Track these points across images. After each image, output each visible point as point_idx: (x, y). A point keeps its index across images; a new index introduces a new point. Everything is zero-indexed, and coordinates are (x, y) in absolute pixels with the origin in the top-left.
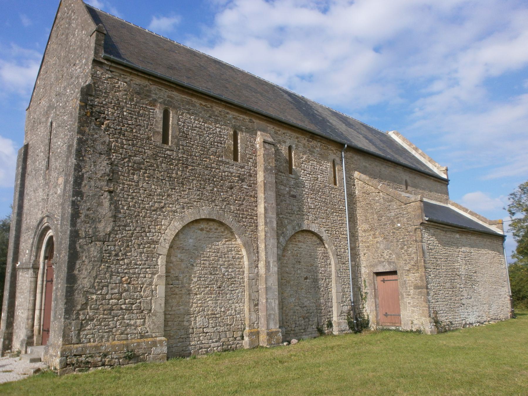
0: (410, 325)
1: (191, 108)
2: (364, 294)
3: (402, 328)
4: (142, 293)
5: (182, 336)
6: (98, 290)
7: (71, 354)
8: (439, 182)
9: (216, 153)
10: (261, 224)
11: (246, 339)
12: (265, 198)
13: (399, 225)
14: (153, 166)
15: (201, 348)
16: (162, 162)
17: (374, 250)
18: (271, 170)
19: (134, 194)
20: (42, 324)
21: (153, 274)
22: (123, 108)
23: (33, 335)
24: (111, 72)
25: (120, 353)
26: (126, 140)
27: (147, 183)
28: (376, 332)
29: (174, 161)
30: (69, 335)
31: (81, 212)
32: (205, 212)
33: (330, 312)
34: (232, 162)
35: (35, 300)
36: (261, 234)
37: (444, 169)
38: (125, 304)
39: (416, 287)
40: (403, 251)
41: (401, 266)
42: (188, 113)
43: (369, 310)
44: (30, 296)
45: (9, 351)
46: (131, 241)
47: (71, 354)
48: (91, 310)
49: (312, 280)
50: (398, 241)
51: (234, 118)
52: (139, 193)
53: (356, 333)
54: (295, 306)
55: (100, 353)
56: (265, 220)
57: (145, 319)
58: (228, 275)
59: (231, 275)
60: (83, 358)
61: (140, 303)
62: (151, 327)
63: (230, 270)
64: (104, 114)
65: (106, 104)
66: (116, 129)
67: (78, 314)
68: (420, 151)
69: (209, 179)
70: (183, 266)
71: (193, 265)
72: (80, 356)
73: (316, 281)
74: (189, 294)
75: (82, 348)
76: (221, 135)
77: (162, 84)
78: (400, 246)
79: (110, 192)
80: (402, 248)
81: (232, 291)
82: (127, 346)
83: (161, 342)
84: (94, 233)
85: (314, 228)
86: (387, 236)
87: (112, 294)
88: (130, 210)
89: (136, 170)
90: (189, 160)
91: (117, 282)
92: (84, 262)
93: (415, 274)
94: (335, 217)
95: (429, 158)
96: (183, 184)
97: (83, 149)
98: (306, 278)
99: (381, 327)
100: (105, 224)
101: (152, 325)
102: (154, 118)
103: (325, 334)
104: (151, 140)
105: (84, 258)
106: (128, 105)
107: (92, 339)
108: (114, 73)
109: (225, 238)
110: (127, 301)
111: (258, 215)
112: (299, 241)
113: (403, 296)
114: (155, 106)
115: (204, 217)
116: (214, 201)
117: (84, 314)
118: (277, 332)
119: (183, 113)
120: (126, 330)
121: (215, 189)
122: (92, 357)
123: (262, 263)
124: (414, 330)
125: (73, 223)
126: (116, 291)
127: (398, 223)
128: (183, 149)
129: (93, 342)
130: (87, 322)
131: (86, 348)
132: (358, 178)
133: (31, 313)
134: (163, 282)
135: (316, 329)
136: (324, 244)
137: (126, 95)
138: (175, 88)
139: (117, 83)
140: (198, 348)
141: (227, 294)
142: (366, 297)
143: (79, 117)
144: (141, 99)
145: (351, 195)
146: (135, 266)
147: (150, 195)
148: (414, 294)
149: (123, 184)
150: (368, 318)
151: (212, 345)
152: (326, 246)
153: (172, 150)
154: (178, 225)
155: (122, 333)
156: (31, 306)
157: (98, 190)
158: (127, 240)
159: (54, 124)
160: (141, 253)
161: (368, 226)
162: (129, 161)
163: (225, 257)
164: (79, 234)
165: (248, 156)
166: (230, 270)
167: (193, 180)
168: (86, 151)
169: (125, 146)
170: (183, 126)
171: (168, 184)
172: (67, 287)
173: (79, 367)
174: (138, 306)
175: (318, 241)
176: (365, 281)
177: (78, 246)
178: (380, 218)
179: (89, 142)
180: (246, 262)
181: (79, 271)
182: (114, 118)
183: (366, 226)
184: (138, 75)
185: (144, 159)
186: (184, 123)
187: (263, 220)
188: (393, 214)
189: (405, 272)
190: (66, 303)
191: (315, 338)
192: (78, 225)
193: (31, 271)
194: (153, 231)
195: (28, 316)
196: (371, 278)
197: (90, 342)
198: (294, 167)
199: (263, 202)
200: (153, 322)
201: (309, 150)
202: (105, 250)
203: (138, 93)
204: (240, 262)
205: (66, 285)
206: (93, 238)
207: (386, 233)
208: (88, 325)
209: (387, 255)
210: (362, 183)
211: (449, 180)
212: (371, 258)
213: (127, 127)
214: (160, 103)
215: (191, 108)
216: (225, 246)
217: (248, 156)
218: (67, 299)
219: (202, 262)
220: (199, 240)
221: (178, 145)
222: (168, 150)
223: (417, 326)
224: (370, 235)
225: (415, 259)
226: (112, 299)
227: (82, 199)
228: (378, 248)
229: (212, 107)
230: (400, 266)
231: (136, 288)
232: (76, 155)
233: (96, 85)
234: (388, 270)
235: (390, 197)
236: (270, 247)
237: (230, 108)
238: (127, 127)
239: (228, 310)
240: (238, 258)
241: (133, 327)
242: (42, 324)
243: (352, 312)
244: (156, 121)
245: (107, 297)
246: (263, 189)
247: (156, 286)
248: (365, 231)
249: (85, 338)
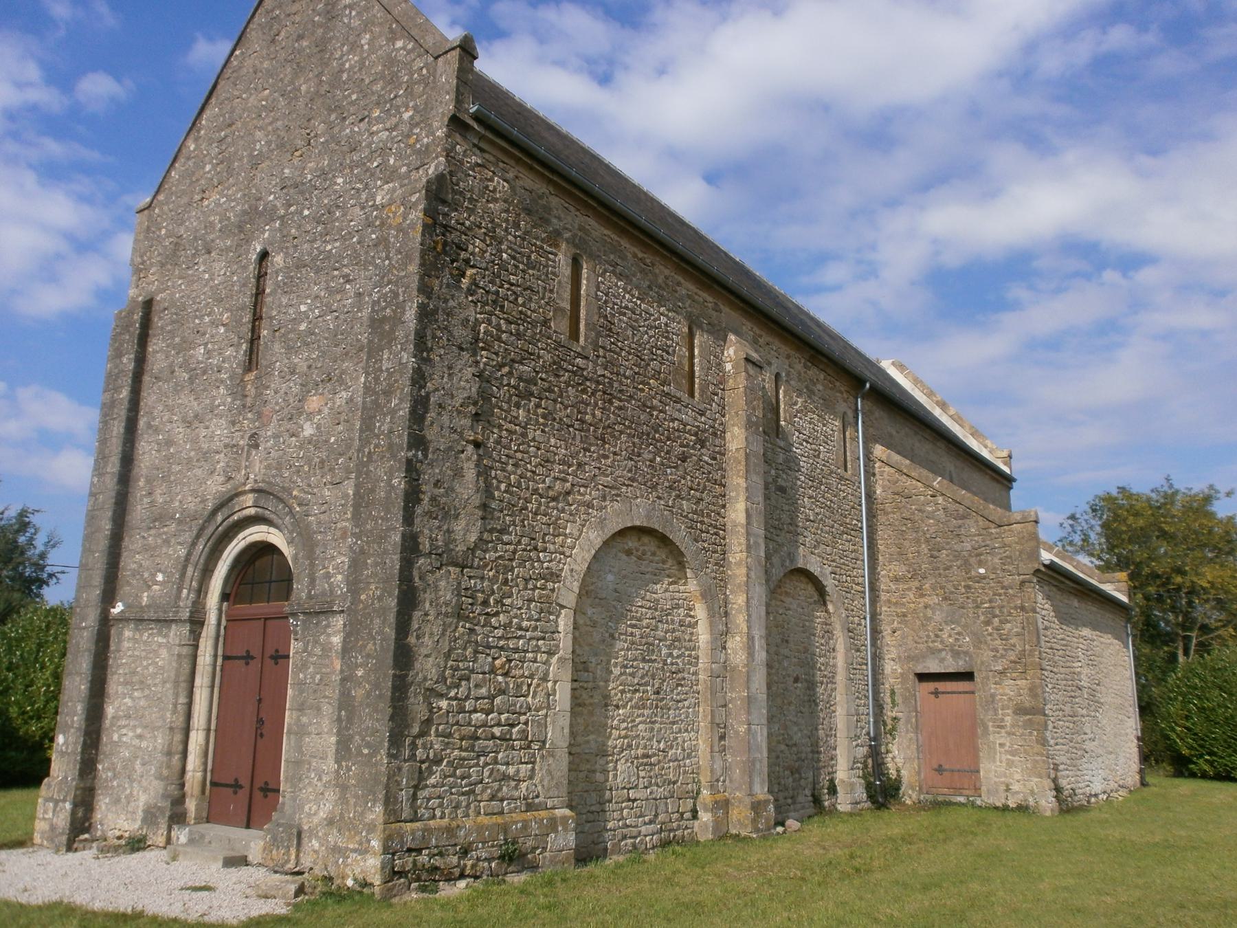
0: (1003, 795)
1: (619, 261)
2: (889, 722)
3: (986, 799)
4: (529, 699)
5: (593, 808)
6: (449, 688)
7: (402, 847)
8: (998, 481)
9: (659, 373)
10: (736, 548)
11: (705, 817)
12: (747, 489)
13: (982, 571)
14: (553, 391)
15: (624, 837)
16: (568, 384)
17: (918, 623)
18: (756, 424)
19: (519, 455)
20: (209, 767)
21: (550, 653)
22: (500, 243)
23: (184, 796)
24: (482, 150)
25: (493, 846)
26: (509, 322)
27: (543, 431)
28: (920, 806)
29: (588, 383)
30: (396, 798)
31: (424, 488)
32: (640, 511)
33: (832, 759)
34: (685, 397)
35: (190, 704)
36: (737, 572)
37: (1005, 454)
38: (499, 724)
39: (1020, 710)
40: (990, 628)
41: (984, 660)
42: (613, 272)
43: (901, 758)
44: (177, 695)
45: (86, 836)
46: (512, 570)
47: (402, 847)
48: (437, 736)
49: (805, 684)
50: (978, 607)
51: (689, 296)
52: (527, 452)
53: (878, 809)
54: (779, 742)
55: (456, 845)
56: (748, 540)
57: (534, 763)
58: (672, 664)
59: (677, 664)
60: (423, 858)
61: (526, 723)
62: (545, 783)
63: (675, 653)
64: (466, 250)
65: (469, 229)
66: (487, 292)
67: (414, 746)
68: (952, 411)
69: (648, 435)
70: (597, 637)
71: (612, 636)
72: (419, 851)
73: (811, 686)
74: (606, 705)
75: (424, 830)
76: (667, 332)
77: (570, 194)
78: (982, 618)
79: (477, 445)
80: (988, 623)
81: (678, 701)
82: (505, 829)
83: (564, 819)
84: (446, 545)
85: (815, 569)
86: (952, 593)
87: (477, 699)
88: (512, 494)
89: (523, 398)
90: (616, 385)
91: (487, 669)
92: (426, 615)
93: (1019, 682)
94: (843, 544)
95: (972, 427)
96: (603, 439)
97: (429, 332)
98: (796, 680)
99: (929, 797)
100: (467, 525)
101: (544, 778)
102: (554, 274)
103: (833, 811)
104: (550, 328)
105: (427, 605)
106: (510, 238)
107: (445, 813)
108: (487, 156)
109: (669, 576)
110: (503, 717)
111: (729, 527)
112: (787, 593)
113: (986, 728)
114: (557, 246)
115: (638, 523)
116: (654, 487)
117: (424, 746)
118: (767, 802)
119: (605, 271)
120: (500, 789)
121: (658, 459)
122: (441, 854)
123: (738, 638)
124: (1012, 805)
125: (408, 519)
126: (483, 691)
127: (980, 566)
128: (605, 357)
129: (441, 818)
130: (429, 768)
131: (427, 830)
132: (884, 458)
133: (178, 737)
134: (567, 675)
135: (810, 798)
136: (825, 604)
137: (507, 211)
138: (594, 208)
139: (491, 180)
140: (620, 837)
141: (669, 709)
142: (894, 729)
143: (422, 250)
144: (533, 227)
145: (870, 496)
146: (520, 633)
147: (547, 461)
148: (1013, 726)
149: (500, 427)
150: (898, 775)
151: (643, 829)
152: (830, 607)
153: (586, 358)
154: (594, 538)
155: (493, 798)
156: (180, 721)
157: (456, 436)
158: (505, 566)
159: (278, 260)
160: (530, 600)
161: (904, 568)
162: (510, 373)
163: (667, 622)
164: (418, 544)
165: (711, 388)
166: (675, 653)
167: (621, 432)
168: (434, 337)
169: (504, 336)
170: (606, 302)
171: (578, 437)
172: (394, 675)
173: (418, 879)
174: (524, 731)
175: (816, 597)
176: (893, 693)
177: (416, 573)
178: (935, 553)
179: (441, 317)
180: (703, 636)
181: (418, 637)
182: (484, 265)
183: (899, 569)
184: (531, 168)
185: (538, 373)
186: (607, 295)
187: (743, 540)
188: (968, 546)
189: (994, 677)
190: (392, 718)
191: (809, 817)
192: (417, 521)
193: (178, 633)
194: (552, 547)
195: (171, 744)
196: (909, 685)
197: (434, 817)
198: (783, 423)
199: (742, 498)
200: (549, 772)
201: (807, 387)
202: (466, 589)
203: (529, 212)
204: (692, 634)
205: (391, 672)
206: (446, 557)
207: (950, 587)
208: (431, 773)
209: (950, 636)
210: (893, 470)
211: (1015, 480)
212: (910, 641)
213: (508, 289)
214: (567, 240)
215: (619, 261)
216: (668, 594)
217: (711, 388)
218: (394, 707)
219: (630, 630)
220: (624, 577)
221: (596, 347)
222: (579, 355)
223: (1021, 796)
224: (910, 589)
225: (1019, 648)
226: (475, 711)
227: (426, 456)
228: (929, 619)
229: (653, 265)
230: (982, 663)
231: (519, 686)
232: (416, 346)
233: (454, 179)
234: (951, 670)
235: (961, 509)
236: (754, 602)
237: (684, 272)
238: (508, 289)
239: (672, 747)
240: (690, 625)
241: (513, 784)
242: (209, 767)
243: (870, 761)
244: (559, 282)
245: (468, 705)
246: (742, 467)
247: (555, 682)
248: (896, 579)
249: (426, 808)
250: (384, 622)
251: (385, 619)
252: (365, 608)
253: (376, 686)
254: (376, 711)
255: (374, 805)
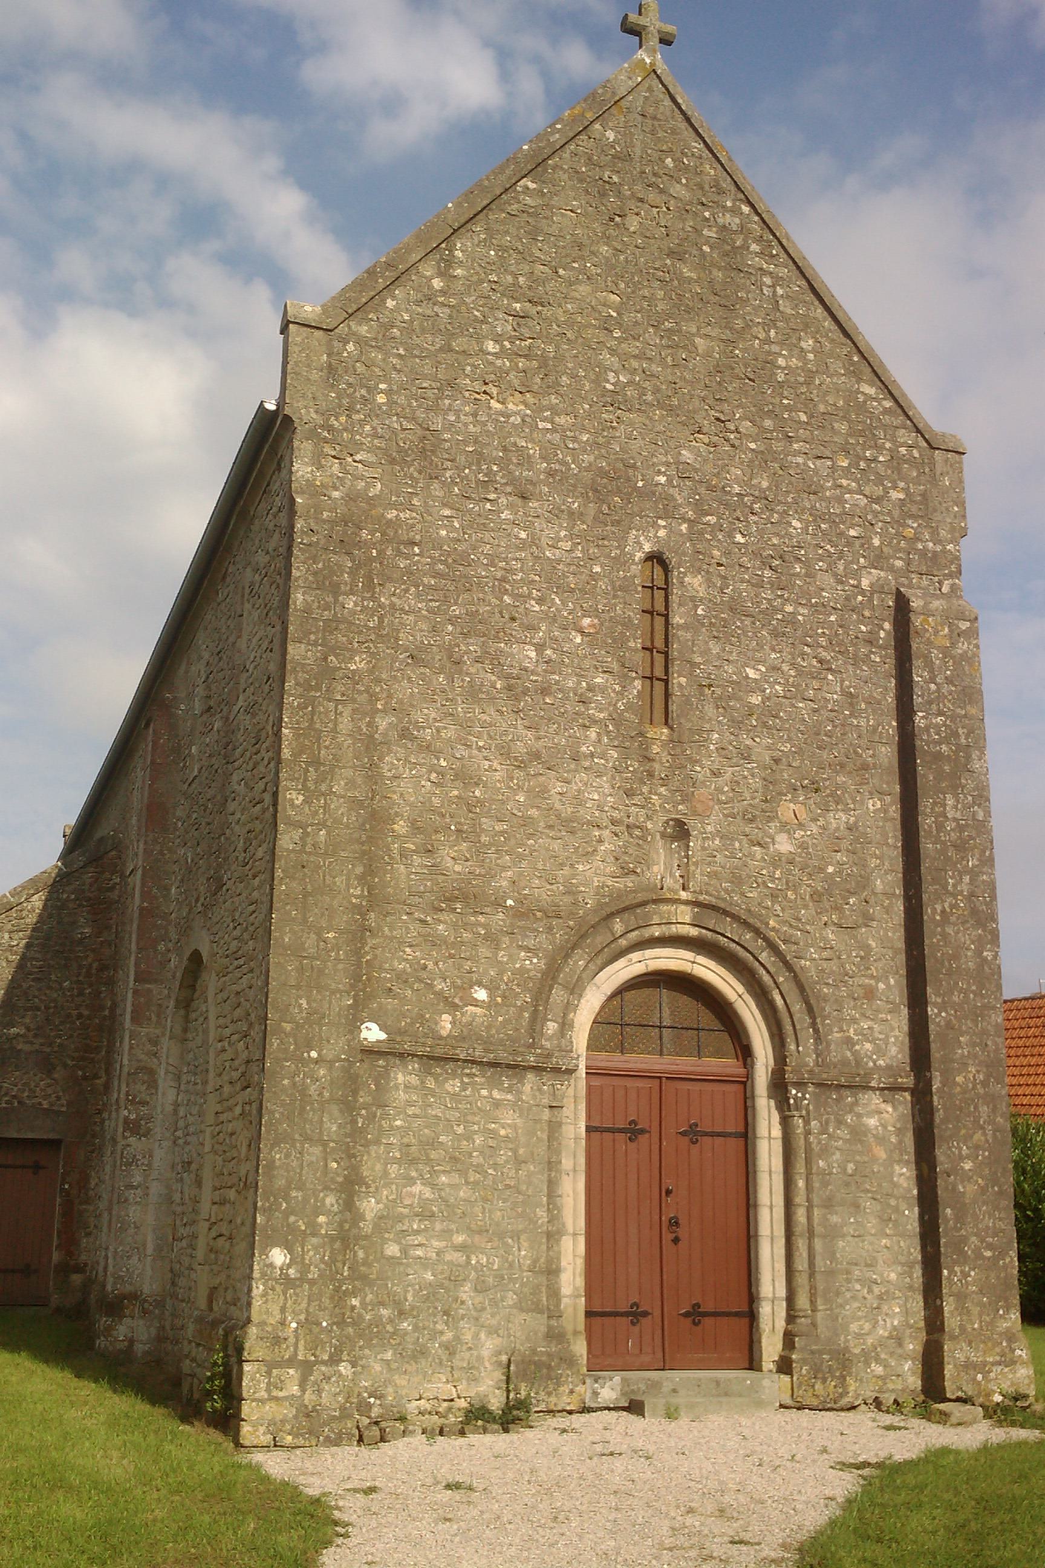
250: (994, 1110)
251: (995, 1107)
252: (964, 1092)
253: (995, 1181)
254: (997, 1208)
255: (1007, 1312)
